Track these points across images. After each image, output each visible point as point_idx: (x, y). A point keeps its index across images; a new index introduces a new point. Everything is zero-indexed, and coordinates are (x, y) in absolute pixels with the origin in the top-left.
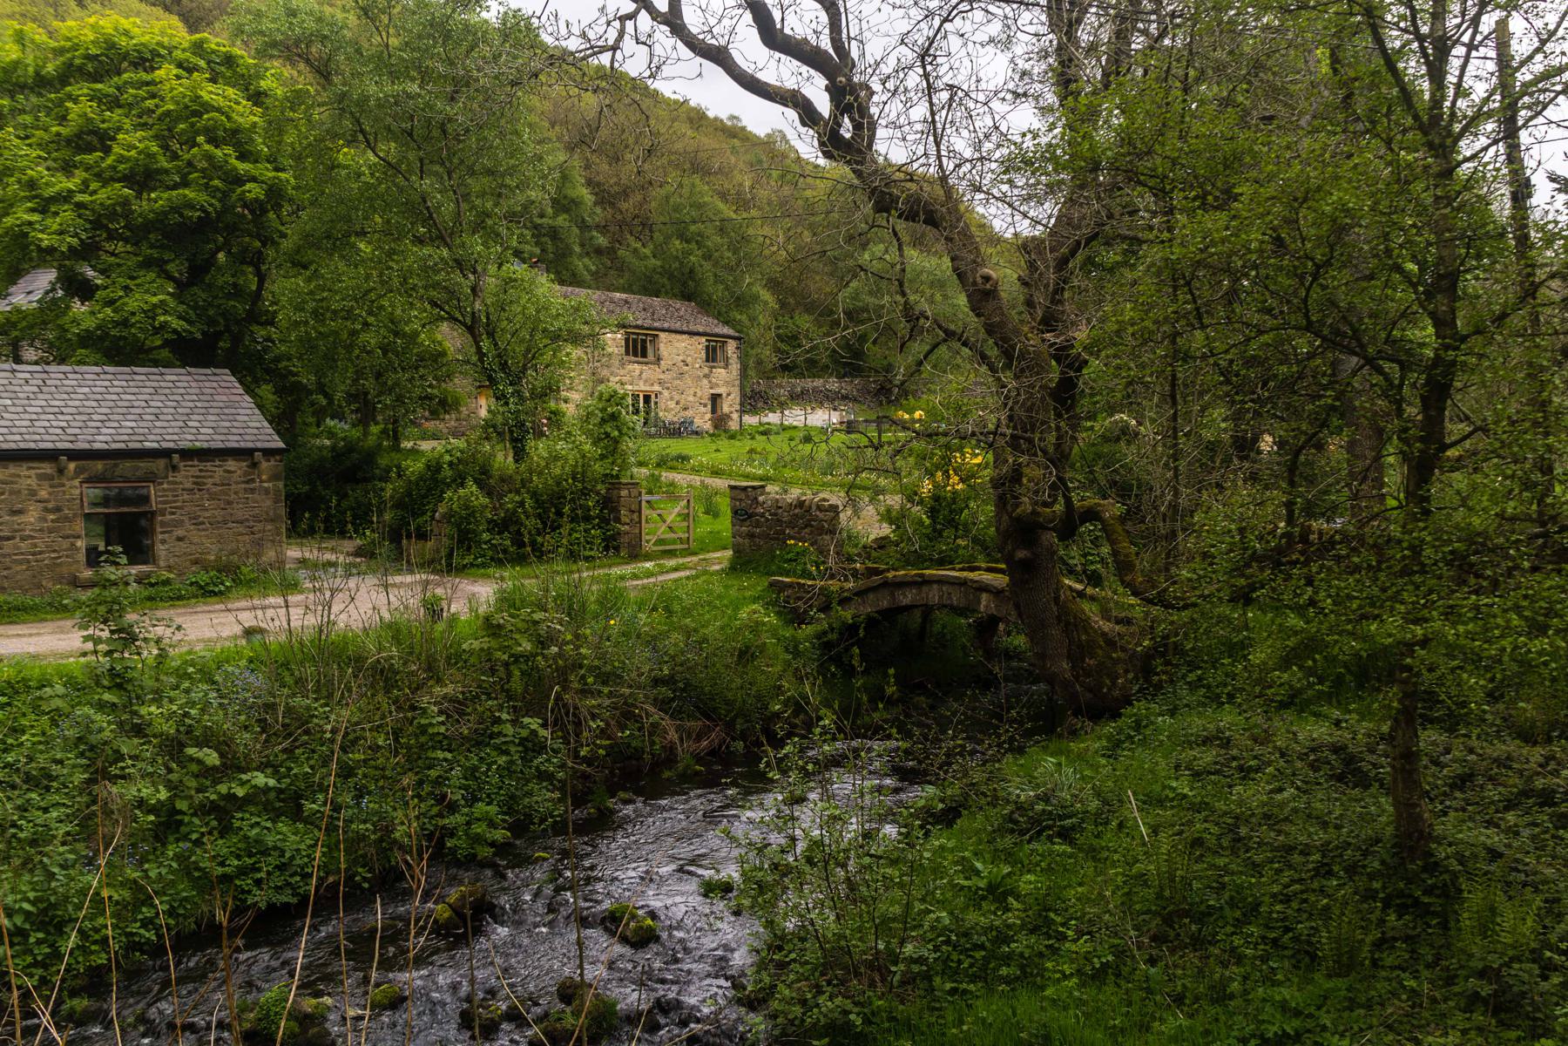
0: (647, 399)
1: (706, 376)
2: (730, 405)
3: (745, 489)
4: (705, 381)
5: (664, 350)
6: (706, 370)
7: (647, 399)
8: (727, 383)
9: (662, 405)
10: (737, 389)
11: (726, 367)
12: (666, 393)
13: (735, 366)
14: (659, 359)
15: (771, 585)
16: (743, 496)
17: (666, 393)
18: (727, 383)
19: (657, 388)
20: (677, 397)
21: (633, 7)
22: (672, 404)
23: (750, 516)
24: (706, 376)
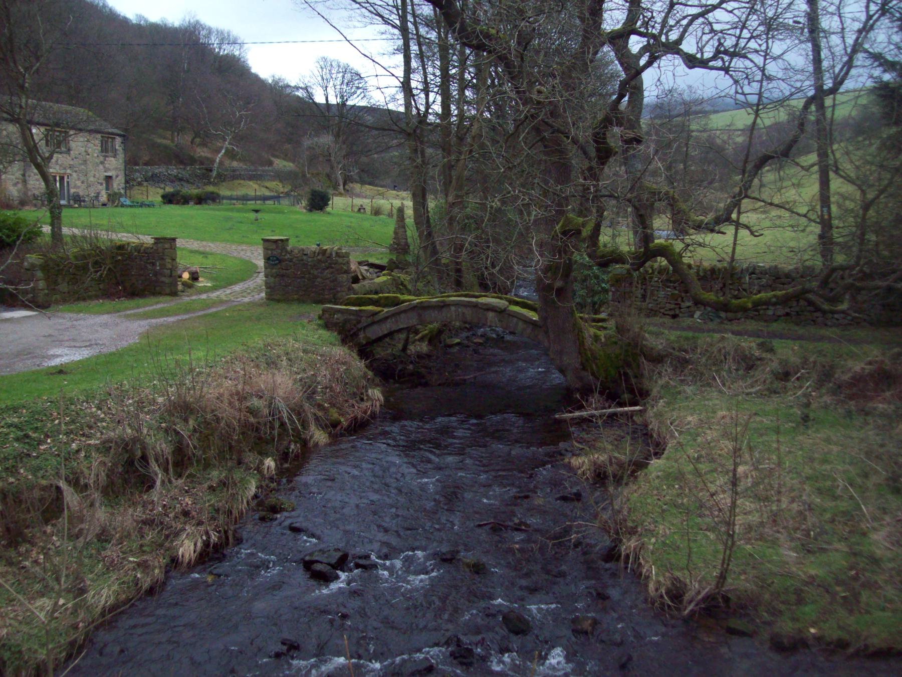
0: (62, 179)
1: (102, 163)
2: (118, 184)
3: (276, 241)
4: (101, 167)
5: (73, 145)
6: (102, 159)
7: (62, 179)
8: (116, 169)
9: (72, 184)
10: (123, 172)
11: (115, 157)
12: (74, 175)
13: (121, 156)
14: (69, 150)
15: (324, 311)
16: (274, 246)
17: (74, 175)
18: (116, 169)
19: (69, 171)
20: (82, 178)
21: (879, 2)
22: (79, 183)
23: (280, 261)
24: (102, 163)
